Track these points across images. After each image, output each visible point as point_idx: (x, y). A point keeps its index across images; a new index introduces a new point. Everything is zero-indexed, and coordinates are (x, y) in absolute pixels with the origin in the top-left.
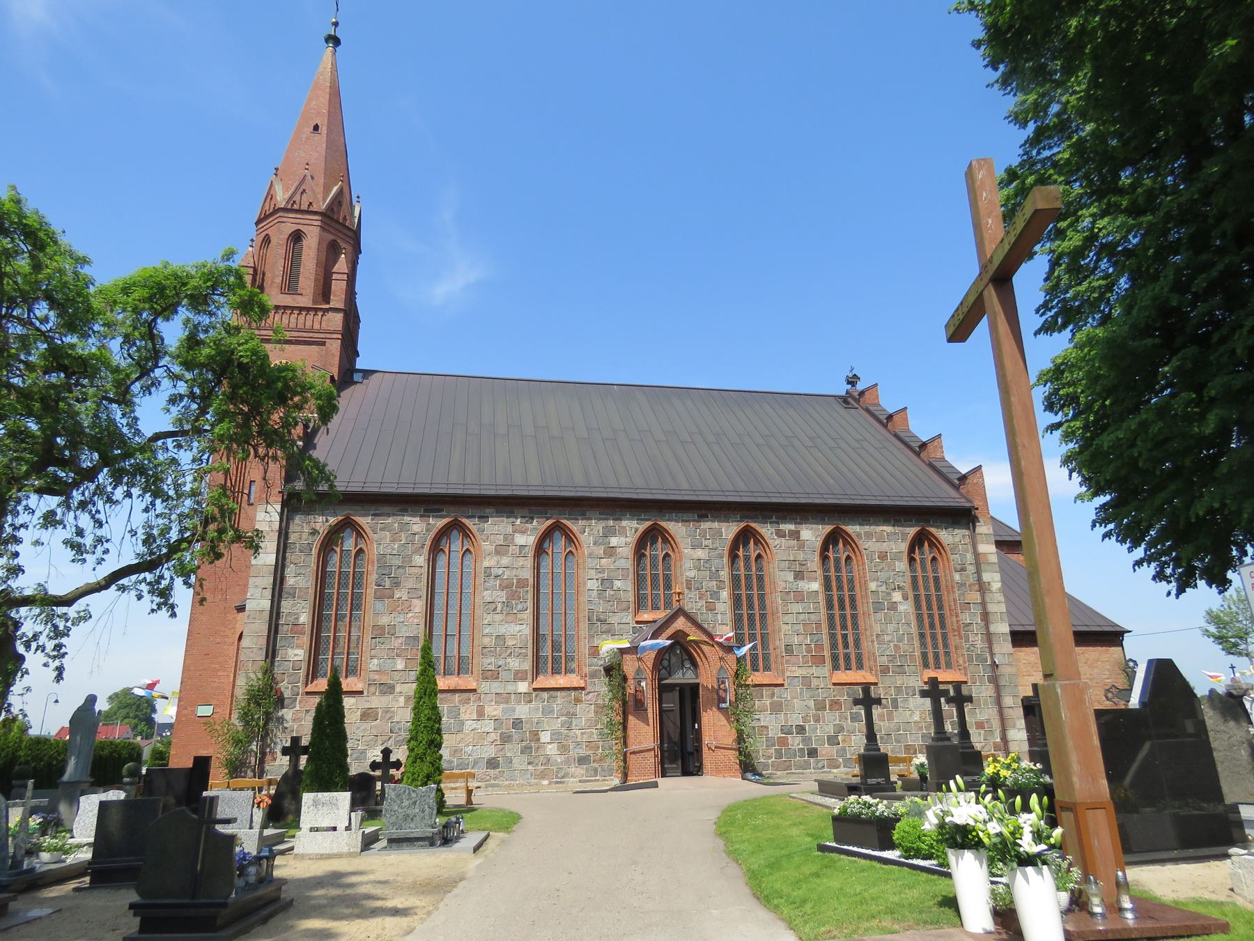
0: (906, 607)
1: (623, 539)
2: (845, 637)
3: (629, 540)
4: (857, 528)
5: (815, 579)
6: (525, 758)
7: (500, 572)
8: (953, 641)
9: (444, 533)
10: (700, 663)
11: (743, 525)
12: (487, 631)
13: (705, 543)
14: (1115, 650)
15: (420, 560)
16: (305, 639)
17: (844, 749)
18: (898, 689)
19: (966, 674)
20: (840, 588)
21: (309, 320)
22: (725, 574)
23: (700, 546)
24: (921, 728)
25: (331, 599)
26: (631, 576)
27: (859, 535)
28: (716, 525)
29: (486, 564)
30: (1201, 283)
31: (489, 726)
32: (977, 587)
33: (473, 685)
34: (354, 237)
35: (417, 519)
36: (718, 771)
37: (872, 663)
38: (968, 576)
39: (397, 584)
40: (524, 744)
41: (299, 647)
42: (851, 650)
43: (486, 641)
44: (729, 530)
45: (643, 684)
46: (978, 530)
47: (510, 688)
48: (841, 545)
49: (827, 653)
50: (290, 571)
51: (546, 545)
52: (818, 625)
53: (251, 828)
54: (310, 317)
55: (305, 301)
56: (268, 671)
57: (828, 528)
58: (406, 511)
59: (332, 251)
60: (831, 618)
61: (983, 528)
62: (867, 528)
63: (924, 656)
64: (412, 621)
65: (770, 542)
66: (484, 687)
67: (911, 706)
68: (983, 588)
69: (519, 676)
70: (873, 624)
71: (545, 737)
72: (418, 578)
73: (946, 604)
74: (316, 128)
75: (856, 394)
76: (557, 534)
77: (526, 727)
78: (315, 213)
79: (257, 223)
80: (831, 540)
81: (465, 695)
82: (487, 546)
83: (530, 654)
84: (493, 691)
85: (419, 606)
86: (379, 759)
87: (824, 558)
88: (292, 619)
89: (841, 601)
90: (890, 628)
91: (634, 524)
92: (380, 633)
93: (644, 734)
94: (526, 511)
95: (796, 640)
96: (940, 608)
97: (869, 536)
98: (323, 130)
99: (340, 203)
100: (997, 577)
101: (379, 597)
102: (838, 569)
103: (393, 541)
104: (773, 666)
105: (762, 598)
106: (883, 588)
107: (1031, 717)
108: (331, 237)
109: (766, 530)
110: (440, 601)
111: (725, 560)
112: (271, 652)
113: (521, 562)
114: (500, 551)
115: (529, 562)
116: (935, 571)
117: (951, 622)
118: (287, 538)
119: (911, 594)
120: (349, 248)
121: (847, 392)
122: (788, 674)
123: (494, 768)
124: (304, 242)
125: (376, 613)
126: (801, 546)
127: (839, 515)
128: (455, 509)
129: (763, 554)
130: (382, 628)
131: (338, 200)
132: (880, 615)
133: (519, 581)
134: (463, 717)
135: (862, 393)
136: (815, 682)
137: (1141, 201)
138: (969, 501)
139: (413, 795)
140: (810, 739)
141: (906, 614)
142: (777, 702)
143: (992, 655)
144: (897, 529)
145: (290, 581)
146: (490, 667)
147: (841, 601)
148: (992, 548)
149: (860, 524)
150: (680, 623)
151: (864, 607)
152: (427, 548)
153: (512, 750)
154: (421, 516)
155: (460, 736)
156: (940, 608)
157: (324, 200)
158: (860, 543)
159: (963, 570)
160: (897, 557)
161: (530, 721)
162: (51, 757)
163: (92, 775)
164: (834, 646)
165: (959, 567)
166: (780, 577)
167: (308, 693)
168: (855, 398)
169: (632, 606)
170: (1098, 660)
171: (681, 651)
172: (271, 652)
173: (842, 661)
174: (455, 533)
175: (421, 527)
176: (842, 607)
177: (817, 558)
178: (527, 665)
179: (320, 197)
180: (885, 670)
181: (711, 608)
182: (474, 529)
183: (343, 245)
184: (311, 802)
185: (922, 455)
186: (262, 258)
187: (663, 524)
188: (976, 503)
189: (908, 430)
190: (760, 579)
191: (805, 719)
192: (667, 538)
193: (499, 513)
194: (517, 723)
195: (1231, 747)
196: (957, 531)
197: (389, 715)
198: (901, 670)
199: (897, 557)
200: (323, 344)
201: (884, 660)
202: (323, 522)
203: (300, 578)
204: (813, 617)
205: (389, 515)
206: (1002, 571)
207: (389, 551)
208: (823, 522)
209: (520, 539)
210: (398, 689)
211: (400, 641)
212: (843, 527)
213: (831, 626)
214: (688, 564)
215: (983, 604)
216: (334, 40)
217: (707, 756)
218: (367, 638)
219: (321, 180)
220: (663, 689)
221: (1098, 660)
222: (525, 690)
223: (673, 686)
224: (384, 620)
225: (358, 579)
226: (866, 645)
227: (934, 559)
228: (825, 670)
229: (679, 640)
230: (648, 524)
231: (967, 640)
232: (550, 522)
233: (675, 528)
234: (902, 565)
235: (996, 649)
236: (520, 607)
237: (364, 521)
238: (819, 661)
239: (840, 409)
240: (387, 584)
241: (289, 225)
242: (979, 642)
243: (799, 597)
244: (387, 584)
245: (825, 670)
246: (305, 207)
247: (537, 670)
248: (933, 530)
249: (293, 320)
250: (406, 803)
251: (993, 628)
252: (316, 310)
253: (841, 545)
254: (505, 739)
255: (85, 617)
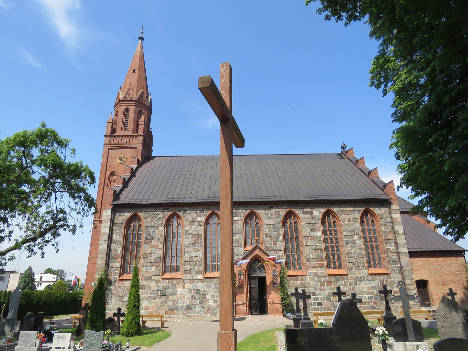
0: (360, 242)
1: (239, 217)
2: (333, 255)
3: (241, 218)
4: (338, 209)
5: (319, 231)
6: (200, 305)
7: (191, 232)
8: (383, 256)
9: (209, 217)
10: (266, 268)
11: (288, 210)
12: (186, 255)
13: (273, 217)
14: (461, 259)
15: (161, 228)
16: (120, 259)
17: (333, 302)
18: (357, 277)
19: (388, 270)
20: (331, 234)
21: (131, 140)
22: (281, 230)
23: (271, 219)
24: (368, 294)
25: (129, 244)
26: (243, 232)
27: (338, 212)
28: (277, 210)
29: (186, 229)
30: (447, 99)
31: (187, 292)
32: (392, 232)
33: (181, 276)
34: (149, 109)
35: (160, 213)
36: (273, 313)
37: (345, 266)
38: (388, 228)
39: (153, 238)
40: (200, 299)
41: (117, 262)
42: (336, 260)
43: (186, 259)
44: (283, 212)
45: (242, 277)
46: (392, 208)
47: (195, 277)
48: (331, 216)
49: (325, 262)
50: (114, 234)
51: (210, 220)
52: (321, 250)
53: (35, 346)
54: (131, 139)
55: (129, 133)
56: (106, 271)
57: (325, 210)
58: (156, 210)
59: (139, 114)
60: (327, 247)
61: (395, 207)
62: (342, 209)
63: (369, 262)
64: (158, 252)
65: (300, 216)
66: (185, 277)
67: (363, 284)
68: (395, 233)
69: (198, 273)
70: (345, 249)
71: (208, 297)
72: (161, 235)
73: (378, 240)
74: (134, 70)
75: (344, 152)
76: (214, 216)
77: (201, 293)
78: (133, 101)
79: (115, 107)
80: (327, 214)
81: (178, 280)
82: (186, 222)
83: (203, 264)
84: (188, 278)
85: (161, 246)
86: (116, 312)
87: (323, 222)
88: (115, 252)
89: (331, 240)
90: (353, 251)
91: (244, 211)
92: (147, 256)
93: (242, 298)
94: (201, 208)
95: (311, 257)
96: (376, 242)
97: (343, 212)
98: (137, 71)
99: (143, 97)
100: (402, 228)
101: (146, 243)
102: (330, 226)
103: (152, 221)
104: (302, 268)
105: (297, 239)
106: (350, 234)
107: (421, 289)
108: (139, 109)
109: (298, 212)
110: (209, 238)
111: (281, 224)
112: (107, 265)
113: (199, 228)
114: (191, 224)
115: (202, 228)
116: (373, 226)
117: (381, 248)
118: (113, 221)
119: (362, 236)
120: (146, 113)
121: (341, 152)
122: (308, 271)
123: (189, 309)
124: (130, 112)
125: (145, 249)
126: (313, 218)
127: (329, 204)
128: (174, 208)
129: (297, 221)
130: (147, 255)
131: (142, 96)
132: (348, 246)
133: (198, 235)
134: (177, 289)
135: (347, 152)
136: (320, 274)
137: (423, 66)
138: (388, 196)
139: (95, 335)
140: (318, 298)
141: (360, 245)
142: (303, 283)
143: (400, 262)
144: (355, 209)
145: (115, 238)
146: (187, 269)
147: (331, 240)
148: (399, 215)
149: (339, 208)
150: (257, 252)
151: (342, 242)
152: (164, 224)
153: (196, 302)
154: (162, 211)
155: (176, 296)
156: (376, 242)
157: (136, 96)
158: (339, 215)
159: (386, 225)
160: (355, 221)
161: (203, 290)
162: (55, 298)
163: (17, 316)
164: (328, 258)
165: (384, 224)
166: (304, 231)
167: (120, 280)
168: (345, 154)
169: (243, 244)
170: (452, 263)
171: (256, 262)
172: (107, 265)
173: (332, 265)
174: (175, 217)
175: (162, 216)
176: (332, 242)
177: (320, 222)
178: (201, 268)
179: (135, 95)
180: (351, 269)
181: (275, 244)
182: (181, 215)
183: (143, 111)
184: (57, 337)
185: (369, 177)
186: (116, 119)
187: (256, 211)
188: (391, 197)
189: (365, 166)
190: (296, 231)
191: (316, 290)
192: (257, 216)
193: (191, 209)
194: (198, 291)
195: (452, 325)
196: (382, 209)
197: (149, 288)
198: (358, 269)
199: (355, 221)
200: (136, 148)
201: (350, 265)
202: (125, 216)
203: (118, 237)
204: (319, 247)
205: (150, 212)
206: (404, 225)
207: (150, 225)
208: (322, 207)
209: (199, 219)
210: (153, 278)
211: (154, 259)
212: (332, 209)
213: (327, 250)
214: (266, 226)
215: (395, 240)
216: (142, 39)
217: (269, 306)
218: (142, 259)
219: (135, 89)
220: (251, 279)
221: (452, 263)
222: (201, 278)
223: (255, 278)
224: (148, 252)
225: (139, 236)
226: (343, 258)
227: (373, 221)
228: (324, 269)
229: (256, 259)
230: (249, 211)
231: (388, 255)
232: (211, 212)
233: (260, 212)
234: (358, 224)
235: (402, 259)
236: (199, 245)
237: (141, 214)
238: (322, 265)
239: (338, 159)
240: (149, 237)
241: (123, 106)
242: (394, 257)
243: (313, 239)
244: (149, 237)
245: (324, 269)
246: (129, 99)
247: (206, 270)
248: (371, 209)
249: (125, 140)
250: (92, 338)
251: (400, 250)
252: (133, 136)
253: (331, 216)
254: (193, 297)
255: (12, 258)
